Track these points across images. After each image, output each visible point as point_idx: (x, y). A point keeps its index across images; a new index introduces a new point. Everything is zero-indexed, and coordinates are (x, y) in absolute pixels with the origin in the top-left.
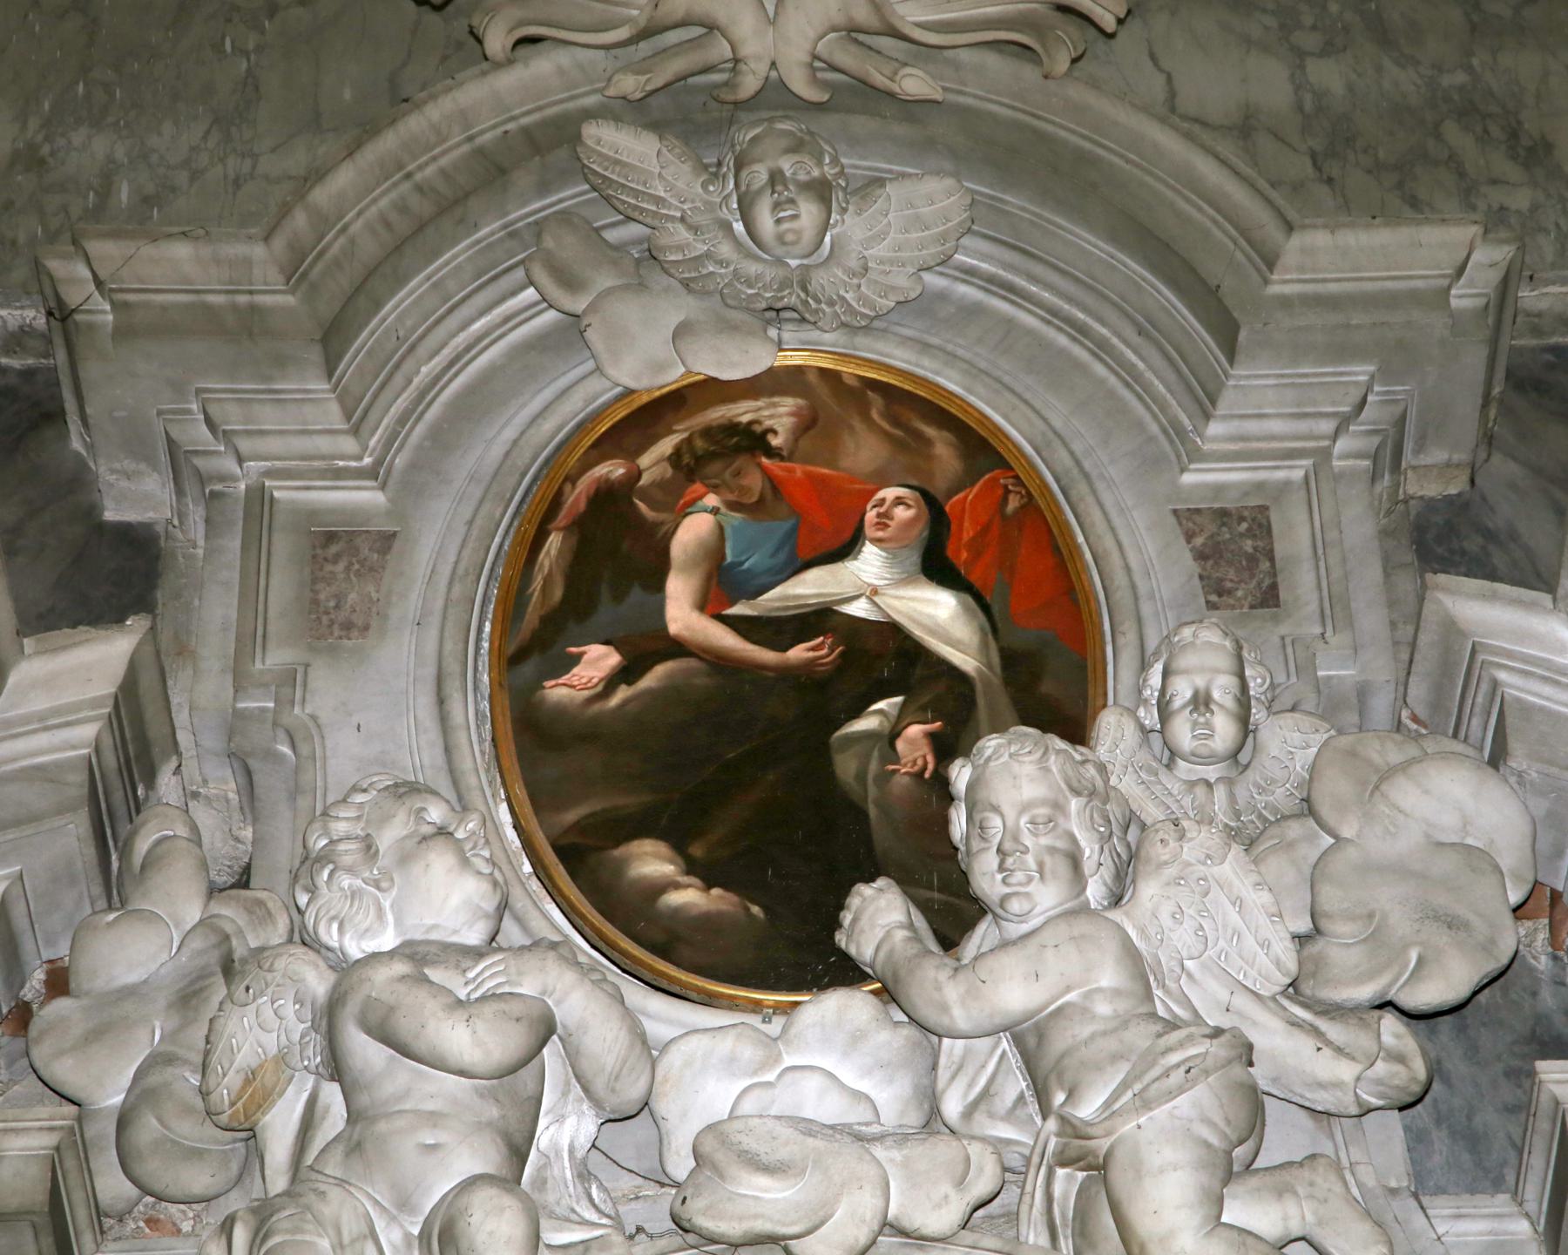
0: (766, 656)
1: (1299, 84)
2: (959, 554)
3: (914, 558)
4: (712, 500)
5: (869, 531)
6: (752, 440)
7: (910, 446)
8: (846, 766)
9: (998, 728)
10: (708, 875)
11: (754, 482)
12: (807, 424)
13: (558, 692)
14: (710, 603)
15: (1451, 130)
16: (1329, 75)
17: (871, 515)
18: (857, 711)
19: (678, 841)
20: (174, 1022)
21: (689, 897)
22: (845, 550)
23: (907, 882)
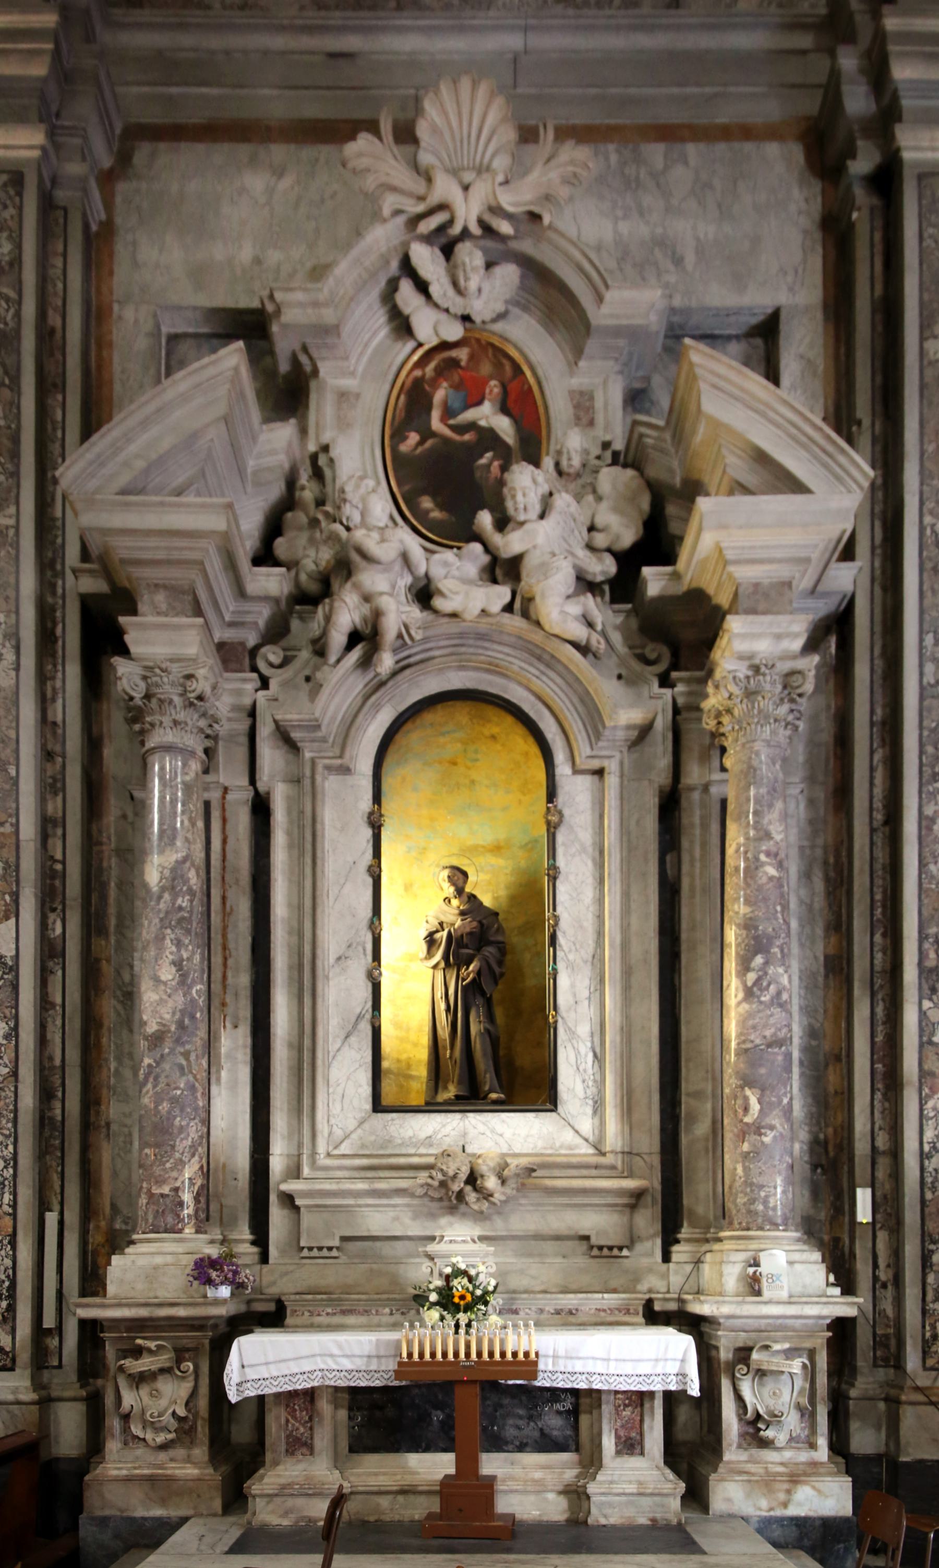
0: (456, 437)
1: (616, 231)
2: (510, 404)
3: (498, 406)
4: (445, 384)
5: (487, 396)
6: (454, 363)
7: (498, 366)
8: (478, 474)
9: (517, 462)
10: (440, 506)
11: (456, 378)
12: (472, 357)
13: (404, 448)
14: (444, 419)
15: (657, 250)
16: (624, 227)
17: (487, 391)
18: (481, 456)
19: (434, 496)
20: (145, 1354)
21: (436, 514)
22: (479, 403)
23: (492, 511)
